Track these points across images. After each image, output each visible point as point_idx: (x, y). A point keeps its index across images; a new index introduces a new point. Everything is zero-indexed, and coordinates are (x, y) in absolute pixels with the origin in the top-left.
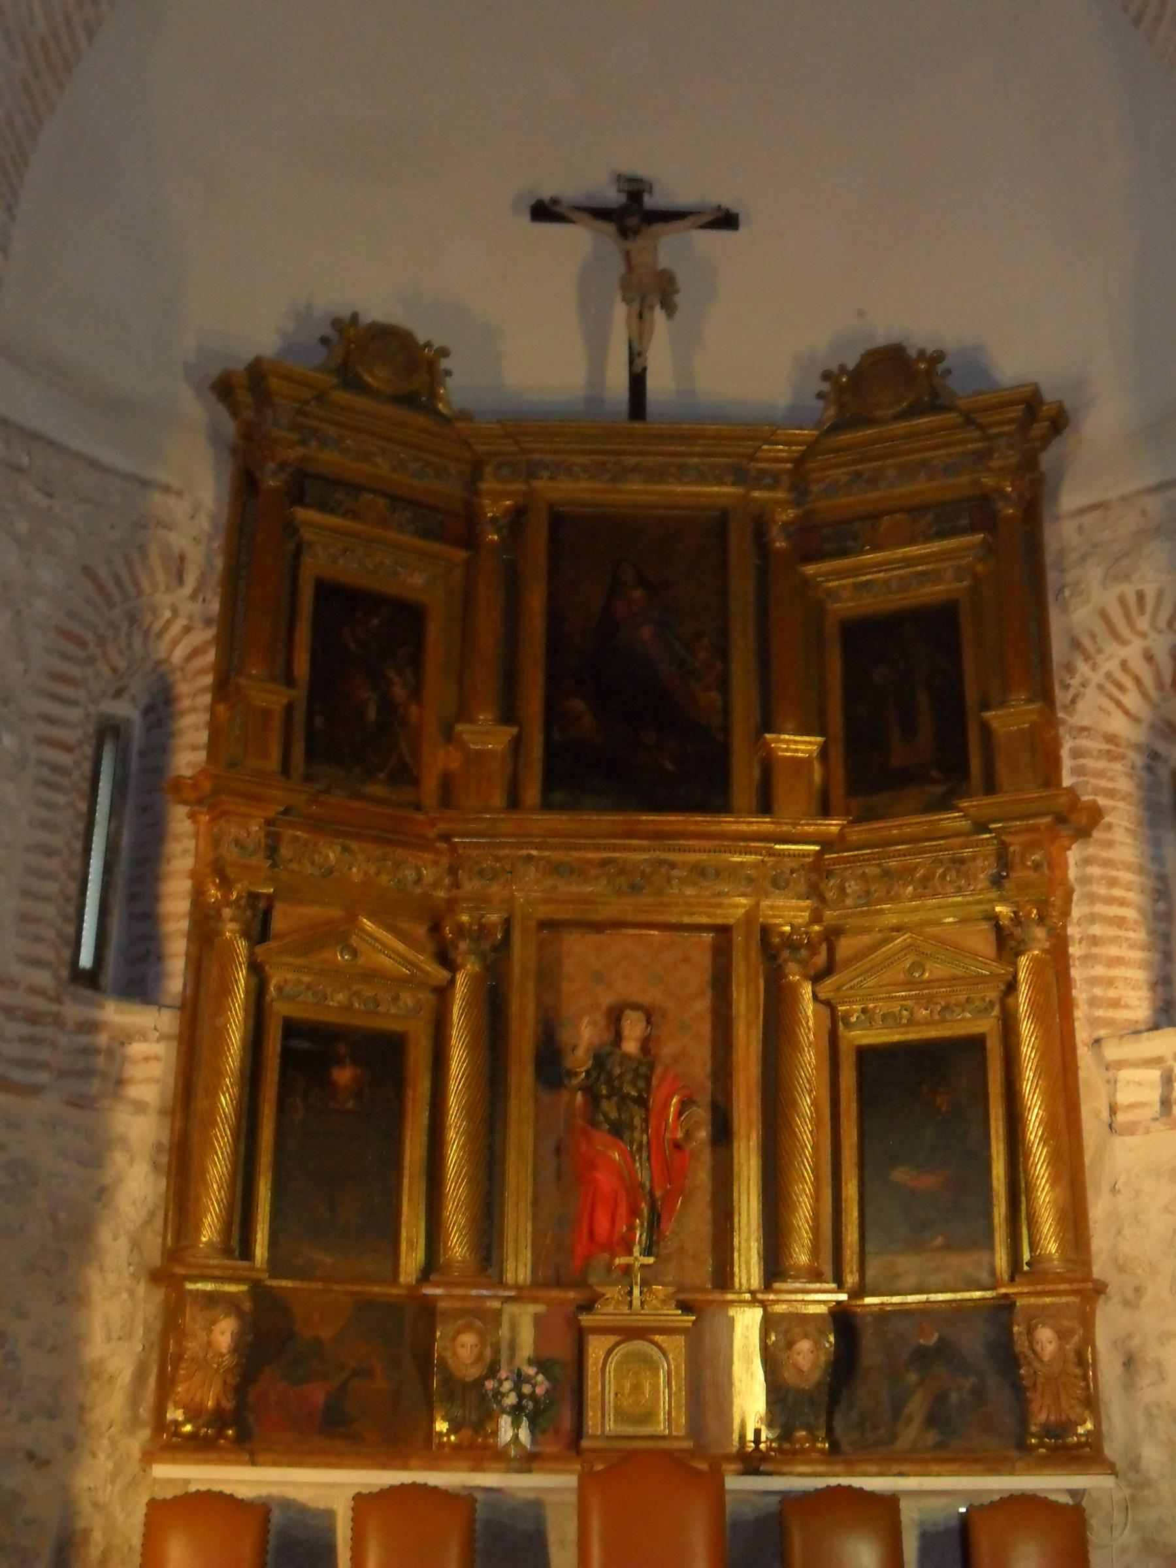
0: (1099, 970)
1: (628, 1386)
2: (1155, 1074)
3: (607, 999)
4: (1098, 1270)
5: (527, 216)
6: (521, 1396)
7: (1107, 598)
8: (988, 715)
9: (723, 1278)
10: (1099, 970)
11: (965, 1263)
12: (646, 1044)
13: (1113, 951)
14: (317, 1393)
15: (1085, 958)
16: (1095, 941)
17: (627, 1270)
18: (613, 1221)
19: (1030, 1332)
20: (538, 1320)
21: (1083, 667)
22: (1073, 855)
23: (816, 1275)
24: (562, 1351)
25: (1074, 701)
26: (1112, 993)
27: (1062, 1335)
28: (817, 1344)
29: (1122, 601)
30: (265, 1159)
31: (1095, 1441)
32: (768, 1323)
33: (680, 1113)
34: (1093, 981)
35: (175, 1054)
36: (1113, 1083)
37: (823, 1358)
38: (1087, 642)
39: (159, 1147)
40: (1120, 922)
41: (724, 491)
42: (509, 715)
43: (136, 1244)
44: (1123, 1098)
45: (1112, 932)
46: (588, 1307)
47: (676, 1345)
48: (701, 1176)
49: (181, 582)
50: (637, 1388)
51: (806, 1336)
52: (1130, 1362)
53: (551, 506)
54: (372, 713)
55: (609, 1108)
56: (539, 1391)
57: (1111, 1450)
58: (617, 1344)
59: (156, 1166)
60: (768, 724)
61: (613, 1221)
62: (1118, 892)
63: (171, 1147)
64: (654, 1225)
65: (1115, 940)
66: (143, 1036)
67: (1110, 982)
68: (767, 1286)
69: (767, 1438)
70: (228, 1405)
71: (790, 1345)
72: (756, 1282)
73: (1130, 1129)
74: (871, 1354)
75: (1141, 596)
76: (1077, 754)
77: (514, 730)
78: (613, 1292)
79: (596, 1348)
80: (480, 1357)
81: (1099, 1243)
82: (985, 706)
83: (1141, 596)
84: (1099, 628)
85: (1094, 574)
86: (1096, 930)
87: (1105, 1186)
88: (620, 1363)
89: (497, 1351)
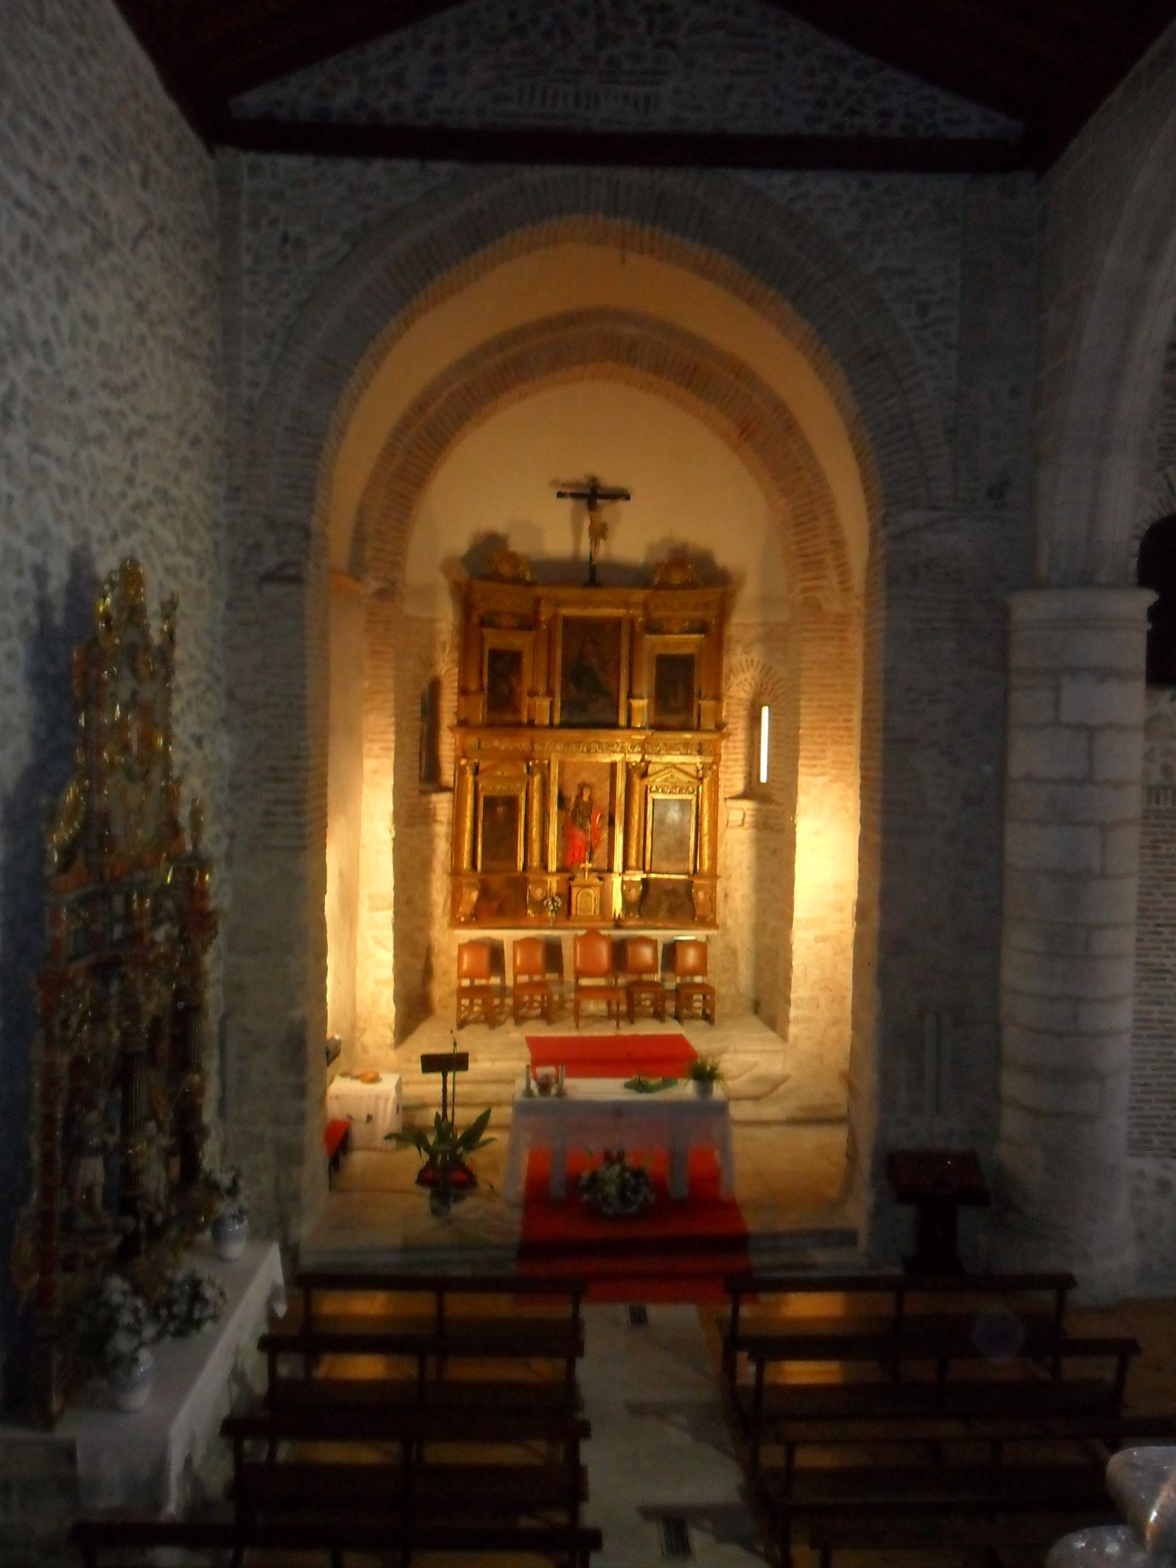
0: (729, 776)
1: (584, 901)
2: (741, 812)
3: (579, 781)
4: (718, 872)
5: (556, 496)
6: (554, 907)
7: (743, 658)
8: (700, 702)
9: (610, 870)
10: (729, 776)
11: (681, 867)
12: (590, 797)
13: (733, 770)
14: (495, 905)
15: (724, 772)
16: (728, 767)
17: (584, 869)
18: (580, 853)
19: (697, 892)
20: (558, 882)
21: (732, 678)
22: (723, 744)
23: (638, 869)
24: (566, 889)
25: (729, 688)
26: (732, 783)
27: (705, 894)
28: (637, 890)
29: (747, 661)
30: (480, 839)
31: (714, 920)
32: (623, 882)
33: (599, 821)
34: (727, 780)
35: (451, 813)
36: (729, 814)
37: (638, 894)
38: (735, 670)
39: (447, 834)
40: (737, 760)
41: (620, 612)
42: (550, 693)
43: (443, 864)
44: (731, 818)
45: (734, 763)
46: (572, 879)
47: (598, 890)
48: (605, 835)
49: (445, 651)
50: (586, 902)
51: (634, 887)
52: (726, 896)
53: (564, 617)
54: (506, 690)
55: (580, 819)
56: (559, 905)
57: (718, 921)
58: (580, 890)
59: (447, 840)
60: (630, 695)
61: (580, 853)
62: (737, 750)
63: (451, 871)
64: (591, 853)
65: (735, 766)
66: (442, 801)
67: (731, 780)
68: (624, 872)
69: (649, 762)
70: (473, 912)
71: (629, 890)
72: (621, 870)
73: (733, 827)
74: (652, 891)
75: (752, 661)
76: (728, 704)
77: (552, 698)
78: (579, 875)
79: (574, 891)
80: (542, 894)
81: (720, 861)
82: (700, 697)
83: (752, 661)
84: (739, 667)
85: (739, 649)
86: (729, 764)
87: (724, 845)
88: (581, 897)
89: (547, 892)
